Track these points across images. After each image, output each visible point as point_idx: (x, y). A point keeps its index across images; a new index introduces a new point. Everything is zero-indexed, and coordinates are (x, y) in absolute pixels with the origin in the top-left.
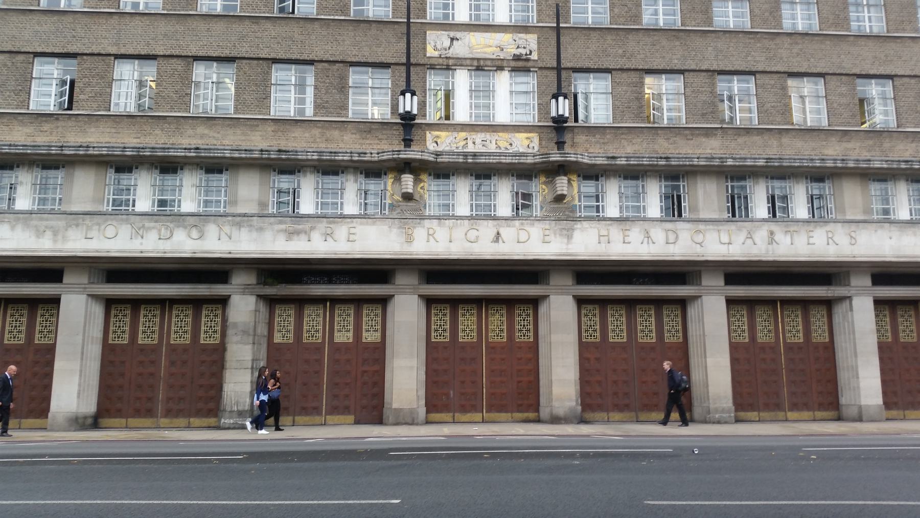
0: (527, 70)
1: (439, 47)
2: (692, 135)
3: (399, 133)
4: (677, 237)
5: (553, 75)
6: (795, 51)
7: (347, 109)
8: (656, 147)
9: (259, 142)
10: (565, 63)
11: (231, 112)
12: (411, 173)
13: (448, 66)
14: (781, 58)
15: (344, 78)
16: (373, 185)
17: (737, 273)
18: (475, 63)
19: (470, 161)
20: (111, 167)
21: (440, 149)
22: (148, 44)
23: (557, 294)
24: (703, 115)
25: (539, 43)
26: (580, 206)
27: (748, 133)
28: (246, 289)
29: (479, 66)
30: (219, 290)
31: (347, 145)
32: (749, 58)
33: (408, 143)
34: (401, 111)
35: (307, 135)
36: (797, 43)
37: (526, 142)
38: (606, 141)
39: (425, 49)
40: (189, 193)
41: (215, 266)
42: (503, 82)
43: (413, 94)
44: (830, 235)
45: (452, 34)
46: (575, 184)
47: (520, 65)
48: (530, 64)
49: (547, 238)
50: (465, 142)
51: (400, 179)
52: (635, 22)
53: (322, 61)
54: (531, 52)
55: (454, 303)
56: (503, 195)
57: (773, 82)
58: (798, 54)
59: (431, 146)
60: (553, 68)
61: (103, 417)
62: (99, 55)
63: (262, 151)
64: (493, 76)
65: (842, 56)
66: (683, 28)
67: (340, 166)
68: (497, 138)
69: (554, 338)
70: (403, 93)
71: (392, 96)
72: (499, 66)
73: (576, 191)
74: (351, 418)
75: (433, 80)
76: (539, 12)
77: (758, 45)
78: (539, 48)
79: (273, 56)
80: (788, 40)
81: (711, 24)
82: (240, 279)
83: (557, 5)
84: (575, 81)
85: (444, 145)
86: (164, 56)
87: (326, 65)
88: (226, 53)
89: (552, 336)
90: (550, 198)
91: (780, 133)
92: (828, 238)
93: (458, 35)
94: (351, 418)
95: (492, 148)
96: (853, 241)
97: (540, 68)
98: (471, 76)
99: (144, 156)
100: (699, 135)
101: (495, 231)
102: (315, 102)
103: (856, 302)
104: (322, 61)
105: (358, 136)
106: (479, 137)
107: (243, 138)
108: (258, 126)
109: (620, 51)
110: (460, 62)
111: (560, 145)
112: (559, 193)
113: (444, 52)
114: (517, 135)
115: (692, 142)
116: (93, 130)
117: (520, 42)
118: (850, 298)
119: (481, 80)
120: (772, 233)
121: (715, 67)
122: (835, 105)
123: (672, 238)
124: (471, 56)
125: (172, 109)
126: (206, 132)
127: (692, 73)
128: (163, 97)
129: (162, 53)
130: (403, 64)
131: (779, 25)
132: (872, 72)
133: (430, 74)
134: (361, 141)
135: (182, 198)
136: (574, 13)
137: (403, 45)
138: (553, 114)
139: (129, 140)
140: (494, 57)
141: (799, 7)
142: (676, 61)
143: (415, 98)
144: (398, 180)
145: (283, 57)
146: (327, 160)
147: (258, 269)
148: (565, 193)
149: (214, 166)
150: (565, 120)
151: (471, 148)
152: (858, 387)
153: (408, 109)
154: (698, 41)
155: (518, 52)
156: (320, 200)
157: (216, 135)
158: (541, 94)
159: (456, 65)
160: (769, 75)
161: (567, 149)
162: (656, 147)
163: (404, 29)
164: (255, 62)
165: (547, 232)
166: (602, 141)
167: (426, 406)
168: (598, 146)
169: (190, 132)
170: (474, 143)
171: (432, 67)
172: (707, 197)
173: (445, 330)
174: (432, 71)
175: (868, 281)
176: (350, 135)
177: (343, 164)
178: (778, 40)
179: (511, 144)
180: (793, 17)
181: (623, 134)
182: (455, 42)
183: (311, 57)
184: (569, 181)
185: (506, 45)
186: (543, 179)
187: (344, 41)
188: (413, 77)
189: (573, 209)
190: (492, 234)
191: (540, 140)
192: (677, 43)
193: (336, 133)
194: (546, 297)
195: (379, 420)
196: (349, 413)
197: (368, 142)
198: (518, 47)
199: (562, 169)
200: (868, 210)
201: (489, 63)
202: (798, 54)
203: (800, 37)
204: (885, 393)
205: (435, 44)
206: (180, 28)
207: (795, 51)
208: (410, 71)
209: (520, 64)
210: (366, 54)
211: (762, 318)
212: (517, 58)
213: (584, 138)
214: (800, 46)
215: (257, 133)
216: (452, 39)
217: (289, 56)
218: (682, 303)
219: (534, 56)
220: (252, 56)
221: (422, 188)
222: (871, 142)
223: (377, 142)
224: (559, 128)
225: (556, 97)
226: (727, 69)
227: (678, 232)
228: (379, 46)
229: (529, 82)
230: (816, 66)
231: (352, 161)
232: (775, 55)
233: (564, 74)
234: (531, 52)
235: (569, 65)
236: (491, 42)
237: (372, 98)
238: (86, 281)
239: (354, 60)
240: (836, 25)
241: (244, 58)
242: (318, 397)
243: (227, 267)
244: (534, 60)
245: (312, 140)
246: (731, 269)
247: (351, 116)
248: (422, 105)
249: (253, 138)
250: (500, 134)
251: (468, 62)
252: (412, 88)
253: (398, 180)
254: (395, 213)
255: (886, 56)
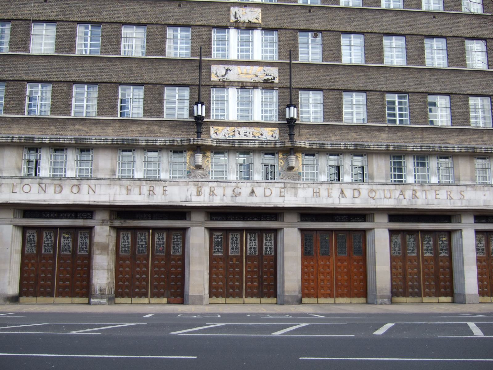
0: (272, 88)
1: (219, 75)
2: (371, 130)
3: (194, 128)
4: (360, 193)
5: (287, 92)
6: (432, 79)
7: (162, 113)
8: (349, 137)
9: (111, 134)
10: (294, 85)
11: (94, 116)
12: (200, 153)
13: (224, 85)
14: (424, 84)
15: (161, 94)
16: (178, 158)
17: (395, 215)
18: (240, 84)
19: (236, 145)
20: (26, 148)
21: (218, 137)
22: (47, 74)
23: (288, 227)
24: (377, 118)
25: (279, 73)
26: (303, 173)
27: (403, 129)
28: (103, 222)
29: (242, 86)
30: (89, 223)
31: (163, 137)
32: (405, 84)
33: (199, 134)
34: (195, 114)
35: (139, 129)
36: (434, 75)
37: (271, 133)
38: (319, 133)
39: (210, 76)
40: (71, 163)
41: (121, 209)
42: (258, 95)
43: (203, 104)
44: (449, 193)
45: (227, 67)
46: (300, 159)
47: (267, 85)
48: (275, 85)
49: (282, 194)
50: (233, 133)
51: (194, 156)
52: (337, 61)
53: (148, 84)
54: (274, 78)
55: (227, 230)
56: (258, 162)
57: (419, 99)
58: (434, 82)
59: (213, 136)
60: (287, 88)
61: (22, 296)
62: (18, 81)
63: (113, 139)
64: (252, 92)
65: (461, 83)
66: (366, 65)
67: (158, 148)
68: (253, 130)
69: (286, 254)
70: (197, 104)
71: (190, 104)
72: (255, 85)
73: (301, 164)
74: (165, 300)
75: (214, 94)
76: (280, 53)
77: (411, 76)
78: (279, 76)
79: (119, 81)
80: (428, 73)
81: (382, 62)
82: (100, 216)
83: (290, 50)
84: (301, 95)
85: (221, 135)
86: (56, 81)
87: (151, 86)
88: (93, 79)
89: (285, 253)
90: (285, 168)
91: (422, 130)
92: (447, 195)
93: (230, 67)
94: (165, 300)
95: (250, 137)
96: (462, 197)
97: (280, 88)
98: (238, 92)
99: (45, 143)
100: (374, 130)
101: (251, 189)
102: (144, 109)
103: (464, 233)
104: (148, 84)
105: (169, 129)
106: (243, 130)
107: (102, 131)
108: (110, 124)
109: (328, 78)
110: (231, 84)
111: (291, 136)
112: (291, 165)
113: (221, 78)
114: (265, 128)
115: (370, 135)
116: (15, 126)
117: (268, 72)
118: (461, 230)
119: (245, 94)
120: (415, 191)
121: (384, 89)
122: (456, 113)
123: (356, 194)
124: (238, 80)
125: (61, 114)
126: (81, 127)
127: (371, 92)
128: (56, 107)
129: (55, 80)
130: (197, 85)
131: (423, 63)
132: (478, 93)
133: (213, 91)
134: (171, 132)
135: (67, 167)
136: (301, 54)
137: (197, 74)
138: (287, 117)
139: (37, 134)
140: (252, 81)
141: (436, 52)
142: (361, 85)
143: (204, 107)
144: (193, 156)
145: (126, 82)
146: (151, 145)
147: (110, 210)
148: (294, 165)
149: (84, 148)
150: (295, 120)
151: (237, 137)
152: (464, 284)
153: (200, 113)
154: (374, 73)
155: (266, 78)
156: (146, 169)
157: (86, 129)
158: (280, 103)
159: (228, 86)
160: (417, 94)
161: (296, 138)
162: (349, 137)
163: (198, 64)
164: (109, 85)
165: (283, 190)
166: (317, 133)
167: (209, 294)
168: (314, 136)
169: (71, 128)
170: (239, 133)
171: (215, 86)
172: (380, 167)
173: (221, 248)
174: (215, 89)
175: (471, 220)
176: (164, 129)
177: (160, 147)
178: (423, 73)
179: (262, 135)
180: (432, 58)
181: (329, 129)
182: (228, 72)
183: (142, 82)
184: (297, 157)
185: (259, 73)
186: (281, 156)
187: (162, 71)
188: (203, 92)
189: (299, 175)
190: (249, 190)
191: (279, 132)
192: (362, 74)
193: (156, 128)
194: (281, 229)
195: (182, 302)
196: (164, 297)
197: (175, 133)
198: (267, 75)
199: (292, 151)
200: (473, 178)
201: (249, 84)
202: (434, 82)
203: (436, 71)
204: (480, 287)
205: (218, 72)
206: (66, 65)
207: (432, 79)
208: (201, 91)
209: (268, 85)
210: (175, 79)
211: (411, 242)
212: (266, 81)
213: (306, 131)
214: (436, 77)
215: (110, 128)
216: (227, 70)
217: (129, 81)
218: (275, 231)
219: (277, 81)
220: (108, 81)
221: (207, 161)
222: (476, 136)
223: (180, 133)
224: (289, 126)
225: (289, 106)
226: (392, 90)
227: (361, 191)
228: (182, 74)
229: (274, 95)
230: (445, 89)
231: (165, 145)
232: (420, 82)
233: (294, 92)
234: (274, 78)
235: (298, 86)
236: (250, 72)
237: (177, 104)
238: (12, 217)
239: (167, 83)
240: (457, 65)
241: (103, 83)
242: (146, 287)
243: (372, 212)
244: (276, 83)
245: (142, 132)
246: (477, 214)
247: (165, 118)
248: (208, 110)
249: (108, 131)
250: (255, 128)
251: (236, 84)
252: (202, 101)
253: (193, 156)
254: (191, 177)
255: (487, 83)
